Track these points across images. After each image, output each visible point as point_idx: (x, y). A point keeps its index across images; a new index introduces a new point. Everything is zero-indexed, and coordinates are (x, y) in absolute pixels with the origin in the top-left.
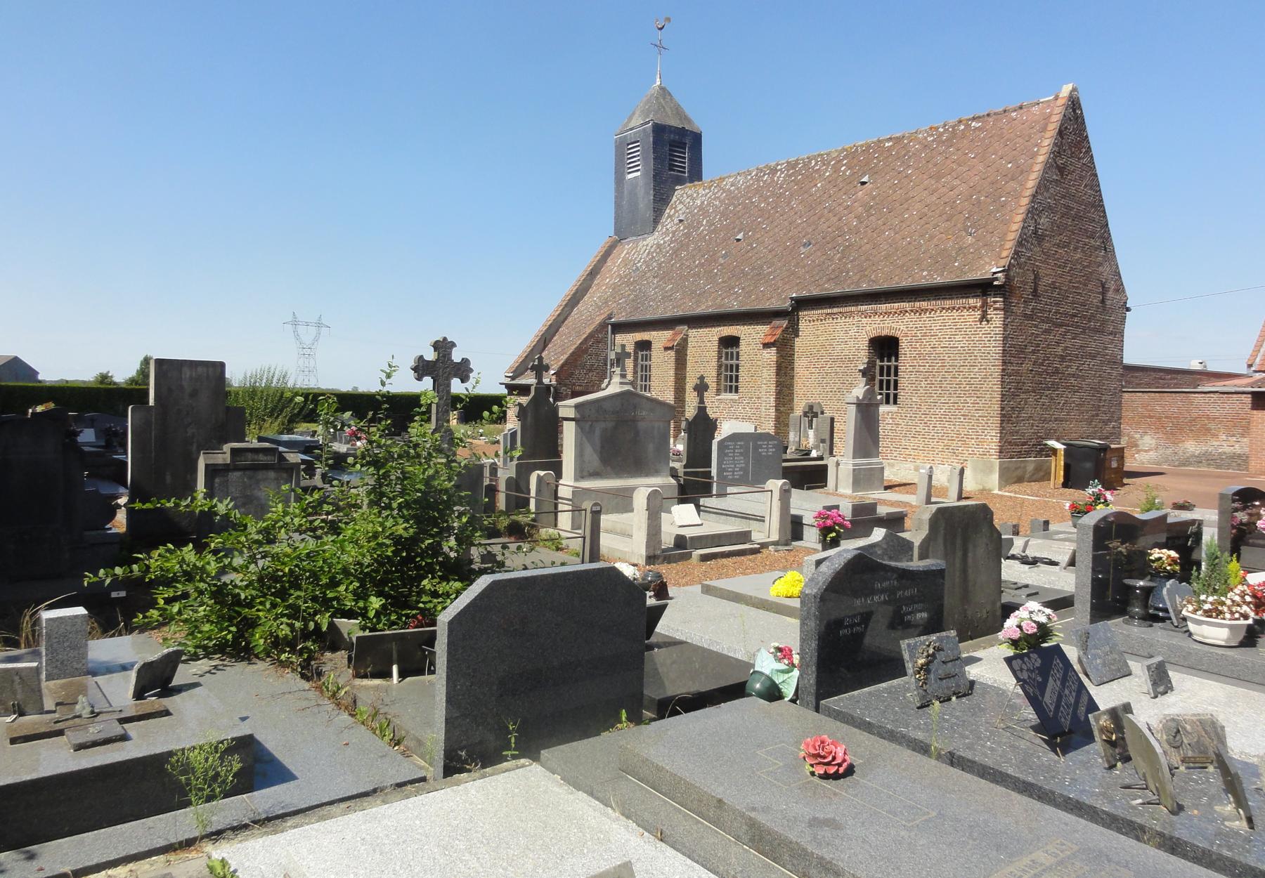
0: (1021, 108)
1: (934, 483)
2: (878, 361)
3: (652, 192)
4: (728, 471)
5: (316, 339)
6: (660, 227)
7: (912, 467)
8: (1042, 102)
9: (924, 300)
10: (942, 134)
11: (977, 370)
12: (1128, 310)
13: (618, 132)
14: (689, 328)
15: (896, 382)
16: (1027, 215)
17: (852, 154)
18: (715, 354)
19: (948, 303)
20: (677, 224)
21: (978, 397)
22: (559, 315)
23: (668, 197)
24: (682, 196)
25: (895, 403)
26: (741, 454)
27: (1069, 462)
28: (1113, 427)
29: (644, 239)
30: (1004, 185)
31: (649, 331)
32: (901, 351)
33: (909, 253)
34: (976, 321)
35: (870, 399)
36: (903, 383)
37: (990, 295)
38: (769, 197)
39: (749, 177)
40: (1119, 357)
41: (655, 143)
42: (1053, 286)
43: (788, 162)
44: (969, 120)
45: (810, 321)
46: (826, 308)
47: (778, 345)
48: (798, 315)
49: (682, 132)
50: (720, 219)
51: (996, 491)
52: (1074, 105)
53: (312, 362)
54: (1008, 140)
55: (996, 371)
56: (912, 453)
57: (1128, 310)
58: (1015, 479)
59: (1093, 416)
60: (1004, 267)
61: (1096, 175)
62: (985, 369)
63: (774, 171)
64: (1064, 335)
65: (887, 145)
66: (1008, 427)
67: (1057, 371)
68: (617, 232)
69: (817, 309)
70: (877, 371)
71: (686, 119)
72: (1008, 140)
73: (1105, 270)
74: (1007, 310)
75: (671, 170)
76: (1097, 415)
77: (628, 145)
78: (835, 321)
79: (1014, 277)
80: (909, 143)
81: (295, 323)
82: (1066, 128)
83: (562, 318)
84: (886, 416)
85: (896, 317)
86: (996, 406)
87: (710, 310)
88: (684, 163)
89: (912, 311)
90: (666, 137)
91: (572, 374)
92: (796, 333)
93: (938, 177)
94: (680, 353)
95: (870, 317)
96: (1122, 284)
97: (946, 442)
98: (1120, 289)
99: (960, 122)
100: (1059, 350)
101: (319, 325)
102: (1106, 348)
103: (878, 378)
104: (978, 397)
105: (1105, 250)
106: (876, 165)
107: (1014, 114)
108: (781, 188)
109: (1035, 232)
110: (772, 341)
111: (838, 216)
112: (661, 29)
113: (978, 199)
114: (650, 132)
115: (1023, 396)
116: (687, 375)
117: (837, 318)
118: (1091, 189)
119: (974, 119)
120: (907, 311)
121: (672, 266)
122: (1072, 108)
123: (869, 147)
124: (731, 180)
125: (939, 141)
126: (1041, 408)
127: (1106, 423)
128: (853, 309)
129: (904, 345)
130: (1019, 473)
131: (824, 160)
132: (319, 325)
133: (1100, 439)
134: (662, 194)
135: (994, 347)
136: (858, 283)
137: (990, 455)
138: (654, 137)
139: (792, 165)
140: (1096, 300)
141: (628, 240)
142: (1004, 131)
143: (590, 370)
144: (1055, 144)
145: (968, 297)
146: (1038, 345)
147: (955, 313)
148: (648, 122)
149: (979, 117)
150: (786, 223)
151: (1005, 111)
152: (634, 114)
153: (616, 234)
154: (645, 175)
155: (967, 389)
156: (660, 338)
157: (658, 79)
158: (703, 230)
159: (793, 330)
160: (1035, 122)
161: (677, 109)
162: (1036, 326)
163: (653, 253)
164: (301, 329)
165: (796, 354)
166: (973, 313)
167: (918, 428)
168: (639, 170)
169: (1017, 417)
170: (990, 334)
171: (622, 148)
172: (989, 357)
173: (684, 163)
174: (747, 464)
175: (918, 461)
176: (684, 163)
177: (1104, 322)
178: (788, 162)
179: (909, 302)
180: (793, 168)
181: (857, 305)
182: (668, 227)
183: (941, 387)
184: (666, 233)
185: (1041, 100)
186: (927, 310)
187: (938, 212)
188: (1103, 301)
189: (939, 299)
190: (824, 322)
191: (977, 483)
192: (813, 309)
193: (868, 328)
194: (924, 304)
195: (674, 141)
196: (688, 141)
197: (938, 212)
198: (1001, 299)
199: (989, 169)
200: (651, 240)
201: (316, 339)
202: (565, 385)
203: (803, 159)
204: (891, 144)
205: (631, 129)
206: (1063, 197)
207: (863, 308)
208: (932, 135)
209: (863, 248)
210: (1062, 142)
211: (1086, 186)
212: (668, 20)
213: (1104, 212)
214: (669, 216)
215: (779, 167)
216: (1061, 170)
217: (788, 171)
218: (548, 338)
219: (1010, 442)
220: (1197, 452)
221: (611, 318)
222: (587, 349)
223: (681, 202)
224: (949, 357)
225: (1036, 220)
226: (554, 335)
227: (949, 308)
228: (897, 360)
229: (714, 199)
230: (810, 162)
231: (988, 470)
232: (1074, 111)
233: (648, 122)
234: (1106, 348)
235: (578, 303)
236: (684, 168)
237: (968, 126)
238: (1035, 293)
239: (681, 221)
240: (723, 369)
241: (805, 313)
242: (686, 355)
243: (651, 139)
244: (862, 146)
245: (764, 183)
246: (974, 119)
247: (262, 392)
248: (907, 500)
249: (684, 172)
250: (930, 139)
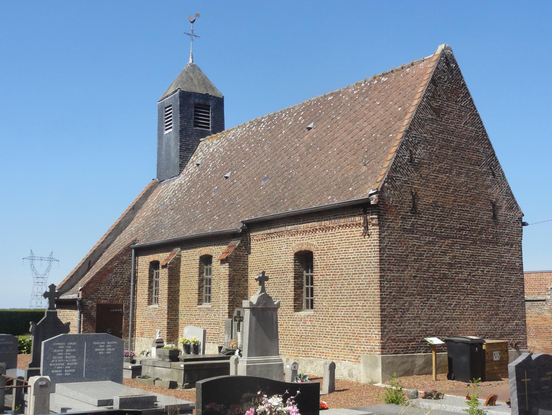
0: (412, 65)
1: (337, 377)
2: (305, 272)
3: (179, 143)
4: (56, 369)
5: (48, 270)
6: (185, 170)
8: (426, 60)
9: (327, 220)
10: (362, 88)
11: (363, 277)
12: (524, 224)
13: (160, 99)
16: (401, 146)
17: (307, 107)
18: (197, 270)
19: (342, 221)
20: (195, 168)
21: (365, 301)
22: (103, 242)
23: (193, 147)
24: (203, 146)
25: (312, 308)
26: (73, 353)
27: (450, 356)
28: (517, 325)
29: (174, 180)
30: (394, 124)
31: (158, 253)
32: (315, 263)
33: (325, 181)
35: (265, 304)
37: (369, 213)
38: (252, 143)
39: (244, 129)
40: (517, 264)
41: (181, 106)
42: (435, 205)
43: (269, 116)
44: (380, 76)
45: (257, 240)
46: (266, 229)
48: (249, 236)
49: (207, 97)
50: (220, 162)
51: (380, 384)
52: (447, 60)
53: (35, 289)
54: (401, 90)
55: (376, 277)
56: (325, 351)
57: (524, 224)
58: (403, 373)
59: (492, 315)
60: (377, 189)
61: (478, 115)
62: (369, 276)
63: (259, 123)
64: (451, 246)
65: (329, 98)
66: (391, 326)
67: (445, 276)
68: (158, 176)
69: (261, 230)
70: (305, 280)
71: (213, 88)
72: (401, 90)
73: (495, 193)
74: (380, 225)
75: (195, 126)
76: (497, 314)
77: (166, 108)
79: (389, 197)
80: (342, 96)
81: (32, 258)
82: (440, 78)
83: (105, 245)
84: (306, 319)
85: (311, 235)
86: (377, 308)
87: (194, 234)
88: (209, 121)
90: (192, 101)
91: (98, 290)
92: (248, 250)
93: (354, 121)
95: (294, 235)
96: (516, 203)
98: (513, 206)
99: (375, 78)
100: (447, 259)
101: (32, 258)
102: (502, 257)
103: (305, 286)
104: (365, 301)
105: (494, 175)
106: (320, 114)
107: (408, 70)
108: (261, 135)
109: (411, 160)
111: (289, 155)
112: (193, 22)
113: (376, 136)
114: (177, 97)
115: (406, 298)
116: (181, 289)
117: (274, 237)
118: (472, 125)
119: (383, 75)
120: (317, 229)
121: (185, 199)
122: (446, 63)
123: (318, 101)
124: (233, 132)
125: (360, 94)
126: (428, 309)
127: (508, 321)
128: (283, 229)
130: (407, 366)
131: (289, 112)
132: (51, 259)
133: (476, 335)
134: (188, 145)
135: (374, 257)
136: (287, 208)
137: (375, 351)
138: (180, 101)
139: (271, 118)
140: (487, 217)
141: (165, 181)
142: (401, 82)
143: (115, 286)
144: (427, 90)
145: (355, 216)
146: (421, 255)
147: (348, 229)
148: (176, 91)
149: (387, 74)
150: (258, 163)
151: (402, 68)
152: (172, 84)
153: (158, 177)
154: (175, 130)
155: (358, 293)
156: (162, 257)
157: (191, 59)
158: (208, 171)
159: (246, 247)
160: (420, 75)
161: (203, 80)
162: (417, 238)
163: (176, 190)
164: (37, 263)
165: (249, 268)
166: (359, 229)
168: (171, 128)
169: (402, 317)
170: (370, 246)
171: (164, 110)
172: (371, 266)
173: (209, 121)
174: (80, 362)
177: (496, 235)
178: (269, 116)
179: (318, 221)
180: (271, 120)
181: (286, 226)
182: (190, 170)
183: (341, 293)
184: (187, 175)
185: (425, 58)
187: (349, 148)
188: (495, 217)
189: (336, 218)
190: (266, 241)
191: (367, 377)
192: (259, 230)
194: (327, 223)
195: (199, 104)
196: (211, 103)
197: (349, 148)
198: (376, 216)
199: (387, 112)
200: (177, 181)
201: (48, 270)
202: (91, 299)
203: (278, 114)
204: (332, 97)
205: (167, 97)
206: (442, 132)
207: (289, 228)
208: (357, 89)
209: (299, 180)
210: (435, 89)
211: (466, 123)
212: (198, 15)
213: (490, 144)
214: (192, 162)
215: (263, 120)
216: (437, 111)
217: (268, 123)
218: (92, 261)
219: (395, 339)
221: (135, 244)
222: (112, 269)
223: (202, 151)
225: (411, 151)
226: (98, 259)
228: (312, 272)
229: (221, 147)
230: (282, 115)
231: (373, 366)
232: (448, 64)
233: (176, 91)
234: (502, 257)
235: (121, 232)
236: (209, 124)
237: (379, 80)
238: (414, 210)
239: (198, 165)
240: (204, 283)
241: (254, 234)
242: (180, 272)
243: (179, 103)
244: (314, 101)
245: (252, 133)
246: (383, 75)
249: (209, 128)
250: (355, 92)
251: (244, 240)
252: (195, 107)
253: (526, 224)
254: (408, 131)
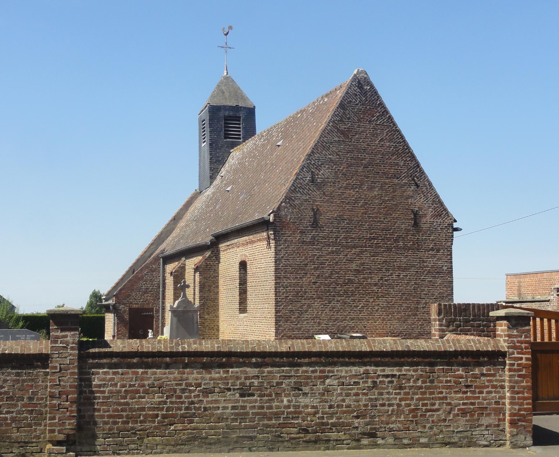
14: (186, 258)
47: (201, 270)
49: (237, 108)
57: (456, 230)
71: (244, 98)
75: (225, 138)
76: (416, 315)
92: (218, 259)
94: (179, 275)
112: (226, 35)
143: (145, 292)
159: (216, 257)
173: (240, 131)
176: (240, 131)
238: (315, 224)
249: (240, 138)
251: (214, 251)
252: (225, 120)
253: (459, 229)
254: (310, 154)
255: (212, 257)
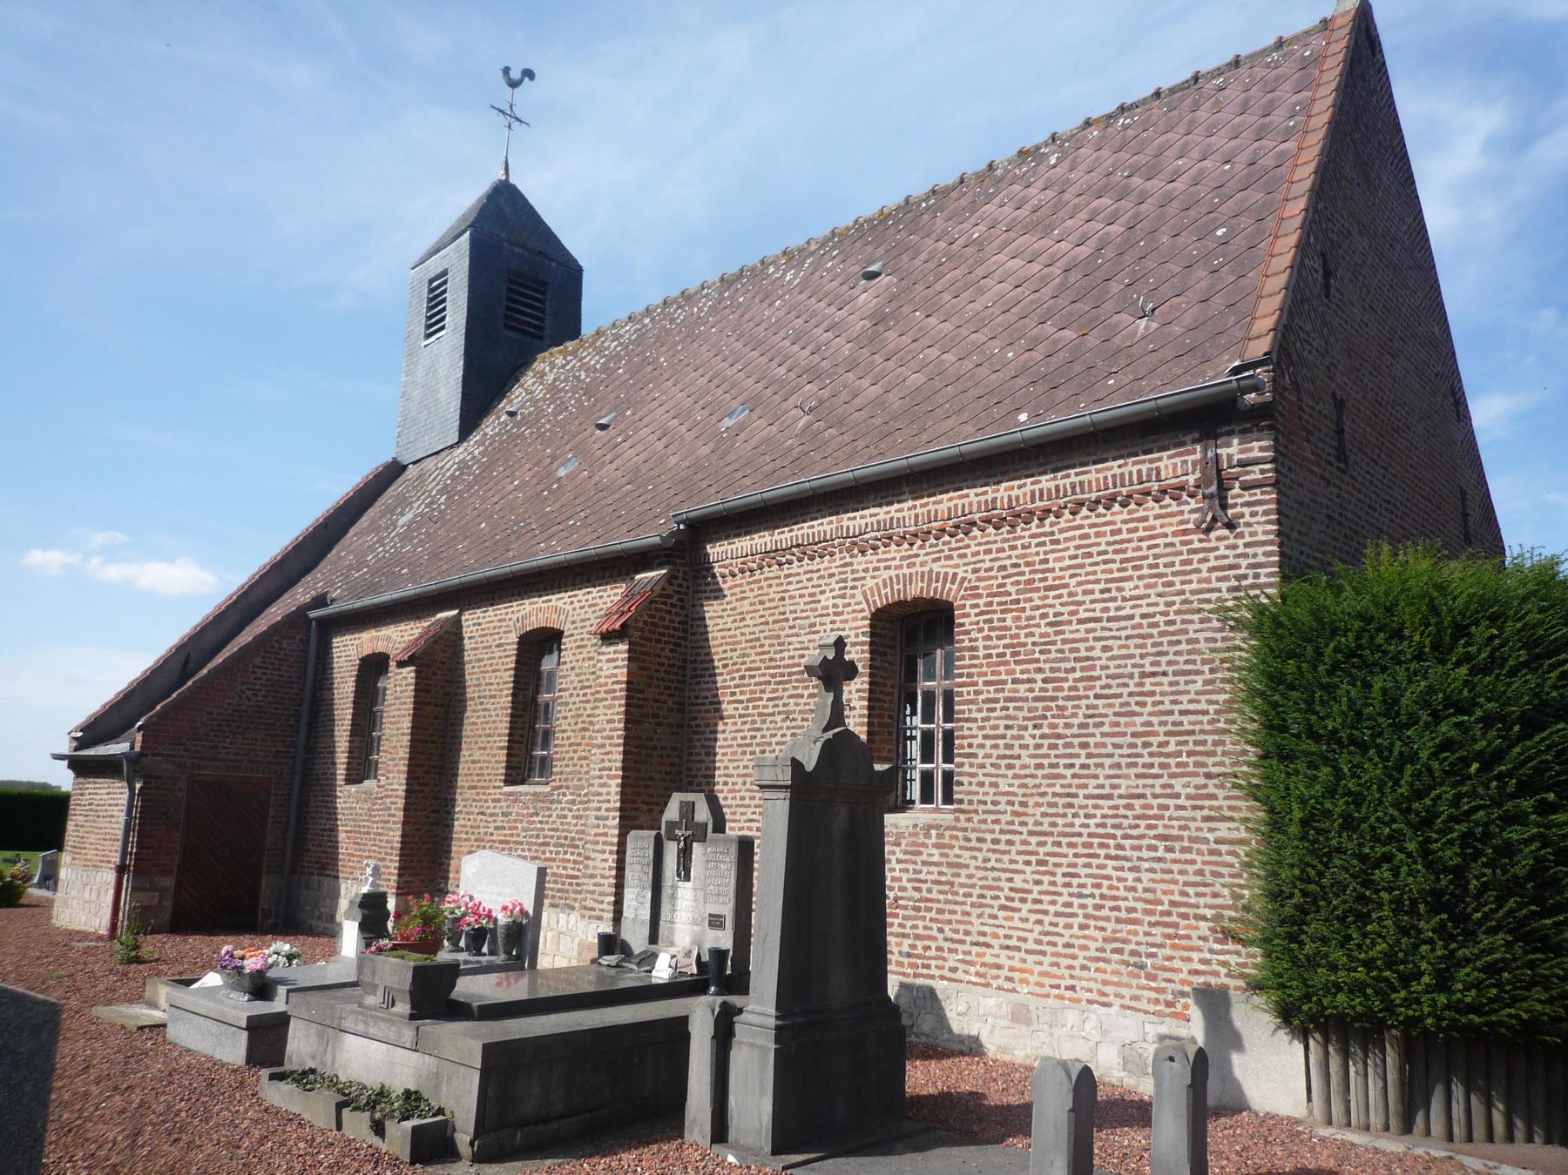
7: (1006, 1009)
15: (949, 737)
25: (948, 798)
34: (1185, 532)
36: (970, 736)
56: (1003, 960)
78: (786, 570)
89: (988, 521)
95: (875, 548)
97: (1110, 926)
110: (617, 626)
117: (790, 562)
120: (973, 524)
129: (967, 619)
147: (1118, 514)
155: (1172, 748)
167: (1018, 882)
175: (1025, 989)
183: (1084, 746)
186: (1031, 513)
193: (870, 583)
212: (529, 74)
220: (574, 916)
224: (1105, 649)
227: (1098, 502)
247: (457, 920)
248: (709, 1030)
251: (676, 578)
252: (510, 281)
255: (670, 597)
